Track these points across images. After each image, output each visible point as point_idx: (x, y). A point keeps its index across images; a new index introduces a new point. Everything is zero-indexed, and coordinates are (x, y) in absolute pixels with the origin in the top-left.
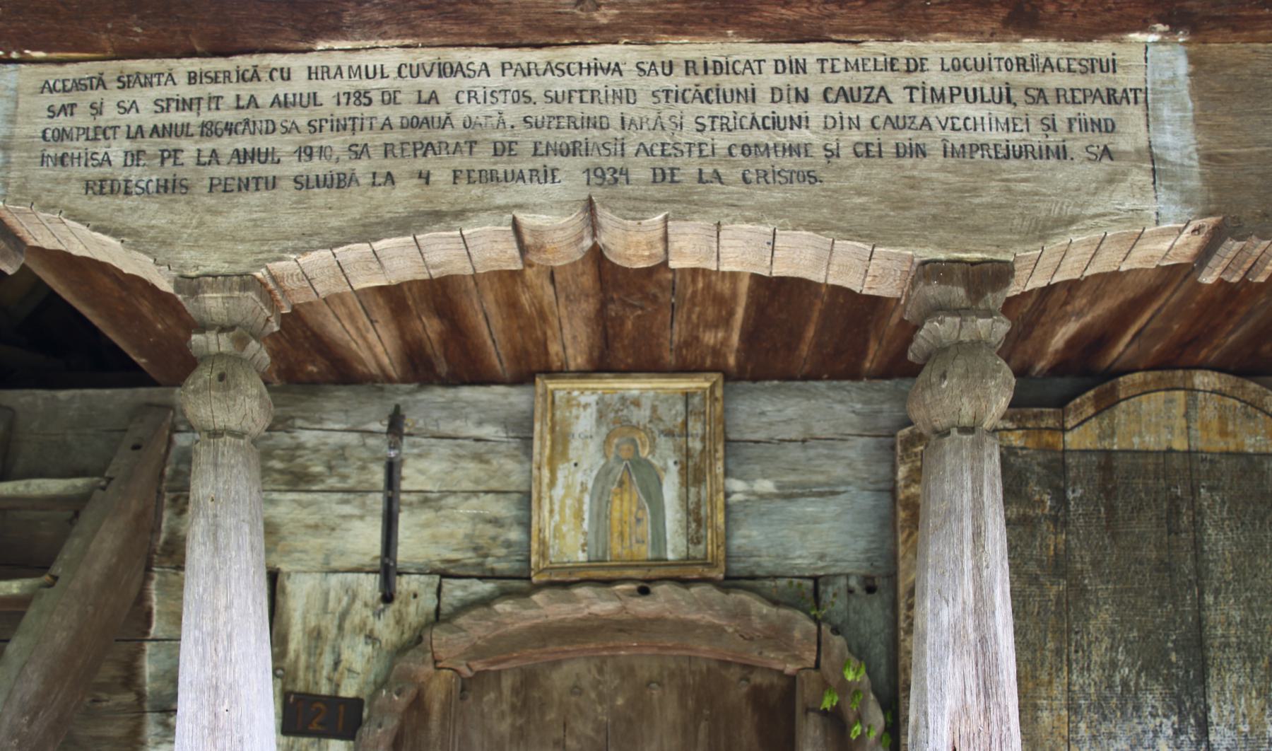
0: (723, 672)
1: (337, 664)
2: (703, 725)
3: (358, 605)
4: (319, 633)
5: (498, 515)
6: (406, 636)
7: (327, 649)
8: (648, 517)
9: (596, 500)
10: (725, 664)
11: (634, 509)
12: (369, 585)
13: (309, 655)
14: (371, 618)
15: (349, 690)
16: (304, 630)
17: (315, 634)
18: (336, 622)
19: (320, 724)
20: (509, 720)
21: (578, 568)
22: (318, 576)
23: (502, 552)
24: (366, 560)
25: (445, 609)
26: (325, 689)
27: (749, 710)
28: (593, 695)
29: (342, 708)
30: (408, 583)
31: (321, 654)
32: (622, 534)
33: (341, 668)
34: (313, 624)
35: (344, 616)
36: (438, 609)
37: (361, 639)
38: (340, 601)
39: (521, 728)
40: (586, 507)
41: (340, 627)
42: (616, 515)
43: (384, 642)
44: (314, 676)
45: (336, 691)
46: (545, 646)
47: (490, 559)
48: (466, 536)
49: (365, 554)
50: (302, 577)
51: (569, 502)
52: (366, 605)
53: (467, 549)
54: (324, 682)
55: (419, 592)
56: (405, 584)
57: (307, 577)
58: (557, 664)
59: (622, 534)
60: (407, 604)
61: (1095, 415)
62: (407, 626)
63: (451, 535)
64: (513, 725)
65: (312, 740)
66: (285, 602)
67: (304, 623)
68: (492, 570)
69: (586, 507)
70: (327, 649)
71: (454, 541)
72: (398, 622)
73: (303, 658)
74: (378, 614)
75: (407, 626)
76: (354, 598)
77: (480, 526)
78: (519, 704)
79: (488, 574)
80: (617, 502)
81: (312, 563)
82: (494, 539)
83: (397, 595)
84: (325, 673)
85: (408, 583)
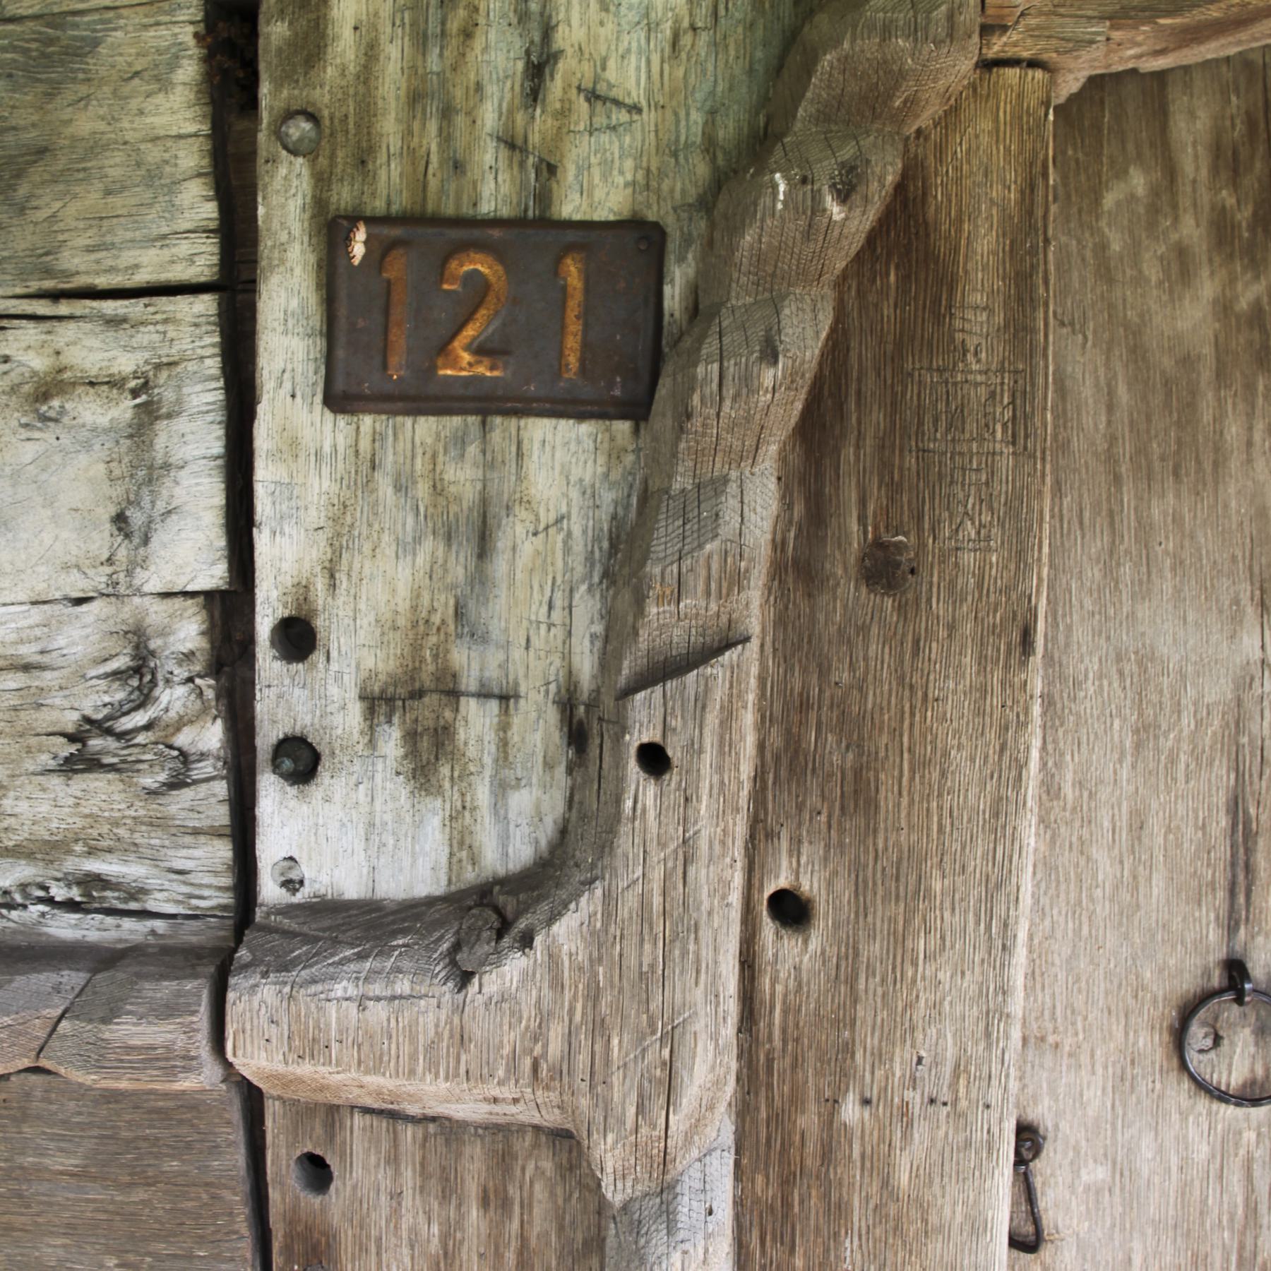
1: (538, 69)
13: (421, 41)
19: (481, 350)
26: (495, 191)
29: (573, 272)
31: (467, 34)
33: (555, 88)
44: (446, 137)
45: (544, 197)
54: (488, 154)
73: (394, 55)
84: (489, 117)
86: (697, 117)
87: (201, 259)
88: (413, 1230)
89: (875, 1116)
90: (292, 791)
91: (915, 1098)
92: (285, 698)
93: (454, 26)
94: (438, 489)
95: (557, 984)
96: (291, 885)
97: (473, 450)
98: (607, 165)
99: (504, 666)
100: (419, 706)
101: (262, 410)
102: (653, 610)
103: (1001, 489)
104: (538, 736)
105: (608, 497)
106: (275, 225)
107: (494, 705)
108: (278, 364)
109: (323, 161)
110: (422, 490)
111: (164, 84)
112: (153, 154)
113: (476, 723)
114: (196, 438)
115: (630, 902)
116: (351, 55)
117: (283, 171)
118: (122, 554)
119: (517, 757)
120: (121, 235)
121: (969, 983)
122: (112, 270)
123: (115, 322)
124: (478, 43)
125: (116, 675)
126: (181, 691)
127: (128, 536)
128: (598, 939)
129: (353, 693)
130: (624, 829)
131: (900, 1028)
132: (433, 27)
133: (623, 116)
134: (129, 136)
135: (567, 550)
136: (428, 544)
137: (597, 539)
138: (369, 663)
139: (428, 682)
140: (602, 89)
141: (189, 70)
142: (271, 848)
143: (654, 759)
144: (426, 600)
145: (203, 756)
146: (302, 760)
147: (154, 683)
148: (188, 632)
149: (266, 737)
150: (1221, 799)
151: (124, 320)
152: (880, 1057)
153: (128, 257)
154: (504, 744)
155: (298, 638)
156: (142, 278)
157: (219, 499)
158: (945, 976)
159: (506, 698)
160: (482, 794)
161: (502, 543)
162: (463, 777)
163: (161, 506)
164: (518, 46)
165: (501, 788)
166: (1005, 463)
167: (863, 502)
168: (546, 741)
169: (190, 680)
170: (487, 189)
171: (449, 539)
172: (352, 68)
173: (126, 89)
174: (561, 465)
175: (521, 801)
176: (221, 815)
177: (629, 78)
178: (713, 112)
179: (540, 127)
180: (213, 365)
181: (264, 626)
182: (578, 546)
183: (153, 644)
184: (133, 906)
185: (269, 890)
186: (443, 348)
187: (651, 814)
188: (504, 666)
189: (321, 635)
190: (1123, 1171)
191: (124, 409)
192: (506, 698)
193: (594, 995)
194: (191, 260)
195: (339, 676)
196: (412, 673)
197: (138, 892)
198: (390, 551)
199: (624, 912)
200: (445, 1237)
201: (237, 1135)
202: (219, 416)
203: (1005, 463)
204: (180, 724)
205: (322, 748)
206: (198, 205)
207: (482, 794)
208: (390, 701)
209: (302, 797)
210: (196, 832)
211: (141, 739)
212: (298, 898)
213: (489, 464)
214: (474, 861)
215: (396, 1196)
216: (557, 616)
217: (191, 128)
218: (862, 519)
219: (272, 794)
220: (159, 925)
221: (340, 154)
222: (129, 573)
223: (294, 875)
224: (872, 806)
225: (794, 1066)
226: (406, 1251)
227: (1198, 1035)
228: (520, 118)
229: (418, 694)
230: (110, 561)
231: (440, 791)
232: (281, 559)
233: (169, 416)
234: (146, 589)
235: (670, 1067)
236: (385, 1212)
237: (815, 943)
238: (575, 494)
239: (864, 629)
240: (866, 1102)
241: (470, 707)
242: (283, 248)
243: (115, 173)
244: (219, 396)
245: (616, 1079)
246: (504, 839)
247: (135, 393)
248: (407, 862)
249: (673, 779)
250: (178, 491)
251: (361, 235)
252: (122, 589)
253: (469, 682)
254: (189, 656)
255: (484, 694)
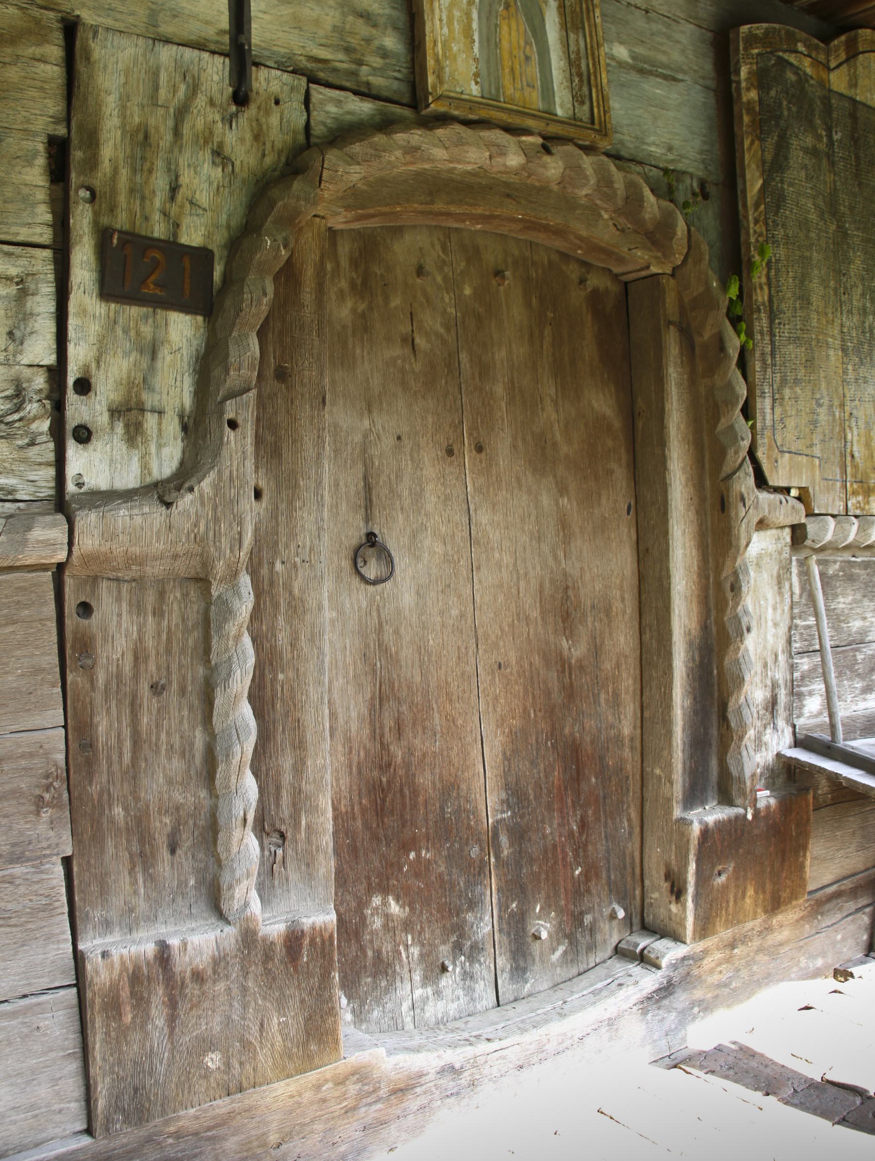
0: (564, 267)
1: (174, 189)
2: (547, 331)
3: (201, 101)
4: (146, 137)
5: (370, 9)
6: (268, 160)
7: (160, 164)
8: (535, 57)
9: (484, 21)
10: (565, 257)
11: (522, 43)
12: (216, 72)
13: (134, 171)
14: (220, 125)
15: (193, 234)
16: (123, 126)
17: (141, 136)
18: (170, 123)
19: (157, 285)
20: (349, 304)
21: (472, 104)
22: (141, 41)
23: (377, 62)
24: (210, 32)
25: (318, 130)
26: (159, 230)
27: (590, 317)
28: (439, 279)
29: (187, 262)
30: (268, 80)
31: (150, 171)
32: (512, 70)
33: (179, 197)
34: (137, 120)
35: (182, 113)
36: (308, 127)
37: (206, 155)
38: (175, 89)
39: (363, 315)
40: (475, 25)
41: (177, 132)
42: (505, 44)
43: (238, 163)
44: (143, 208)
45: (175, 235)
46: (432, 202)
47: (364, 68)
48: (335, 28)
49: (207, 23)
50: (117, 39)
51: (457, 13)
52: (212, 102)
53: (336, 48)
54: (157, 216)
55: (282, 97)
56: (266, 81)
57: (124, 41)
58: (397, 231)
59: (512, 70)
60: (268, 113)
61: (847, 60)
62: (268, 146)
63: (317, 22)
64: (354, 310)
65: (144, 310)
66: (91, 77)
67: (123, 115)
68: (368, 84)
69: (475, 25)
70: (160, 164)
71: (321, 33)
72: (257, 137)
73: (124, 174)
74: (229, 120)
75: (268, 146)
76: (194, 89)
77: (350, 18)
78: (359, 281)
79: (363, 89)
80: (505, 28)
81: (131, 19)
82: (368, 41)
83: (253, 95)
84: (157, 203)
85: (268, 80)
86: (225, 216)
87: (45, 235)
88: (127, 630)
89: (286, 568)
90: (81, 446)
91: (297, 560)
92: (78, 410)
93: (146, 167)
94: (138, 334)
95: (203, 504)
96: (80, 485)
97: (150, 321)
98: (196, 227)
99: (160, 401)
100: (130, 414)
101: (72, 296)
102: (232, 373)
103: (315, 351)
104: (171, 428)
105: (195, 343)
106: (78, 227)
107: (156, 415)
108: (78, 280)
109: (97, 207)
110: (133, 333)
111: (31, 164)
112: (25, 191)
113: (150, 421)
114: (43, 304)
115: (227, 473)
116: (108, 170)
117: (81, 207)
118: (11, 348)
119: (164, 434)
120: (11, 220)
121: (312, 518)
122: (6, 233)
123: (9, 254)
124: (154, 176)
125: (6, 397)
126: (35, 405)
127: (14, 341)
128: (216, 488)
129: (105, 409)
130: (225, 447)
131: (292, 535)
132: (138, 167)
133: (201, 212)
134: (15, 181)
135: (182, 360)
136: (134, 353)
137: (191, 357)
138: (112, 397)
139: (133, 406)
140: (194, 201)
141: (41, 161)
142: (72, 469)
143: (233, 425)
144: (133, 374)
145: (41, 434)
146: (84, 435)
147: (23, 402)
148: (40, 381)
149: (71, 423)
150: (361, 476)
151: (12, 254)
152: (287, 546)
153: (14, 229)
154: (160, 430)
155: (84, 386)
156: (20, 238)
157: (54, 329)
158: (305, 515)
159: (161, 413)
160: (153, 448)
161: (160, 356)
162: (146, 442)
163: (28, 330)
164: (167, 181)
165: (160, 446)
166: (316, 343)
167: (275, 352)
168: (174, 428)
169: (39, 401)
170: (156, 228)
171: (141, 352)
172: (108, 175)
173: (14, 162)
174: (182, 330)
175: (166, 451)
176: (51, 457)
177: (204, 198)
178: (229, 216)
179: (174, 210)
180: (51, 277)
181: (71, 381)
182: (185, 359)
183: (24, 385)
184: (10, 497)
185: (71, 487)
186: (144, 282)
187: (233, 443)
188: (160, 401)
189: (93, 385)
190: (341, 612)
191: (13, 290)
192: (161, 413)
193: (215, 509)
194: (41, 235)
195: (100, 402)
196: (128, 401)
197: (12, 492)
198: (120, 355)
199: (224, 478)
200: (139, 631)
201: (51, 595)
202: (54, 297)
203: (316, 343)
204: (35, 419)
205: (93, 430)
206: (44, 214)
207: (153, 448)
208: (119, 412)
209: (85, 449)
210: (40, 464)
211: (17, 425)
212: (82, 490)
213: (156, 326)
214: (150, 474)
215: (120, 615)
216: (178, 384)
217: (42, 184)
218: (275, 358)
219: (72, 449)
220: (21, 505)
221: (103, 206)
222: (14, 356)
223: (81, 481)
224: (280, 456)
225: (259, 551)
226: (124, 639)
227: (360, 564)
228: (168, 205)
229: (129, 410)
230: (5, 350)
231: (138, 447)
232: (79, 355)
233: (33, 295)
234: (22, 362)
235: (240, 533)
236: (115, 623)
237: (264, 505)
238: (184, 340)
239: (276, 394)
240: (283, 563)
241: (148, 415)
242: (81, 237)
243: (9, 195)
244: (54, 289)
245: (223, 540)
246: (161, 466)
247: (17, 284)
248: (125, 475)
249: (239, 430)
250: (36, 325)
251: (116, 236)
252: (11, 362)
253: (148, 406)
254: (40, 391)
255: (153, 411)
